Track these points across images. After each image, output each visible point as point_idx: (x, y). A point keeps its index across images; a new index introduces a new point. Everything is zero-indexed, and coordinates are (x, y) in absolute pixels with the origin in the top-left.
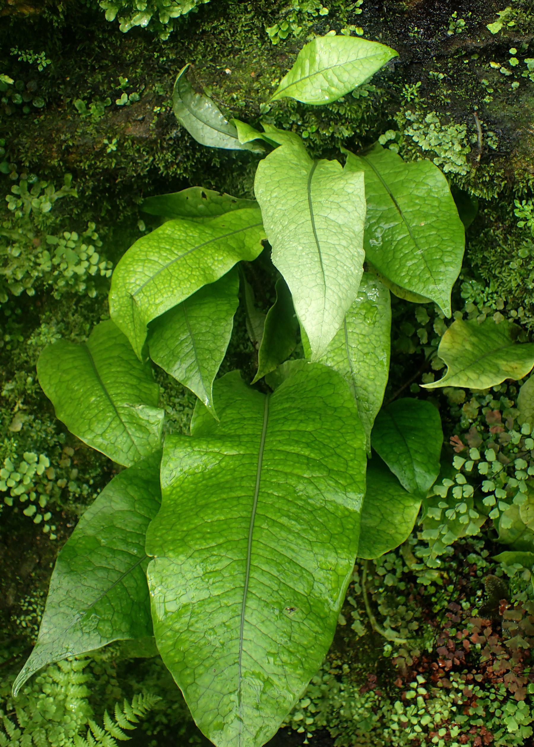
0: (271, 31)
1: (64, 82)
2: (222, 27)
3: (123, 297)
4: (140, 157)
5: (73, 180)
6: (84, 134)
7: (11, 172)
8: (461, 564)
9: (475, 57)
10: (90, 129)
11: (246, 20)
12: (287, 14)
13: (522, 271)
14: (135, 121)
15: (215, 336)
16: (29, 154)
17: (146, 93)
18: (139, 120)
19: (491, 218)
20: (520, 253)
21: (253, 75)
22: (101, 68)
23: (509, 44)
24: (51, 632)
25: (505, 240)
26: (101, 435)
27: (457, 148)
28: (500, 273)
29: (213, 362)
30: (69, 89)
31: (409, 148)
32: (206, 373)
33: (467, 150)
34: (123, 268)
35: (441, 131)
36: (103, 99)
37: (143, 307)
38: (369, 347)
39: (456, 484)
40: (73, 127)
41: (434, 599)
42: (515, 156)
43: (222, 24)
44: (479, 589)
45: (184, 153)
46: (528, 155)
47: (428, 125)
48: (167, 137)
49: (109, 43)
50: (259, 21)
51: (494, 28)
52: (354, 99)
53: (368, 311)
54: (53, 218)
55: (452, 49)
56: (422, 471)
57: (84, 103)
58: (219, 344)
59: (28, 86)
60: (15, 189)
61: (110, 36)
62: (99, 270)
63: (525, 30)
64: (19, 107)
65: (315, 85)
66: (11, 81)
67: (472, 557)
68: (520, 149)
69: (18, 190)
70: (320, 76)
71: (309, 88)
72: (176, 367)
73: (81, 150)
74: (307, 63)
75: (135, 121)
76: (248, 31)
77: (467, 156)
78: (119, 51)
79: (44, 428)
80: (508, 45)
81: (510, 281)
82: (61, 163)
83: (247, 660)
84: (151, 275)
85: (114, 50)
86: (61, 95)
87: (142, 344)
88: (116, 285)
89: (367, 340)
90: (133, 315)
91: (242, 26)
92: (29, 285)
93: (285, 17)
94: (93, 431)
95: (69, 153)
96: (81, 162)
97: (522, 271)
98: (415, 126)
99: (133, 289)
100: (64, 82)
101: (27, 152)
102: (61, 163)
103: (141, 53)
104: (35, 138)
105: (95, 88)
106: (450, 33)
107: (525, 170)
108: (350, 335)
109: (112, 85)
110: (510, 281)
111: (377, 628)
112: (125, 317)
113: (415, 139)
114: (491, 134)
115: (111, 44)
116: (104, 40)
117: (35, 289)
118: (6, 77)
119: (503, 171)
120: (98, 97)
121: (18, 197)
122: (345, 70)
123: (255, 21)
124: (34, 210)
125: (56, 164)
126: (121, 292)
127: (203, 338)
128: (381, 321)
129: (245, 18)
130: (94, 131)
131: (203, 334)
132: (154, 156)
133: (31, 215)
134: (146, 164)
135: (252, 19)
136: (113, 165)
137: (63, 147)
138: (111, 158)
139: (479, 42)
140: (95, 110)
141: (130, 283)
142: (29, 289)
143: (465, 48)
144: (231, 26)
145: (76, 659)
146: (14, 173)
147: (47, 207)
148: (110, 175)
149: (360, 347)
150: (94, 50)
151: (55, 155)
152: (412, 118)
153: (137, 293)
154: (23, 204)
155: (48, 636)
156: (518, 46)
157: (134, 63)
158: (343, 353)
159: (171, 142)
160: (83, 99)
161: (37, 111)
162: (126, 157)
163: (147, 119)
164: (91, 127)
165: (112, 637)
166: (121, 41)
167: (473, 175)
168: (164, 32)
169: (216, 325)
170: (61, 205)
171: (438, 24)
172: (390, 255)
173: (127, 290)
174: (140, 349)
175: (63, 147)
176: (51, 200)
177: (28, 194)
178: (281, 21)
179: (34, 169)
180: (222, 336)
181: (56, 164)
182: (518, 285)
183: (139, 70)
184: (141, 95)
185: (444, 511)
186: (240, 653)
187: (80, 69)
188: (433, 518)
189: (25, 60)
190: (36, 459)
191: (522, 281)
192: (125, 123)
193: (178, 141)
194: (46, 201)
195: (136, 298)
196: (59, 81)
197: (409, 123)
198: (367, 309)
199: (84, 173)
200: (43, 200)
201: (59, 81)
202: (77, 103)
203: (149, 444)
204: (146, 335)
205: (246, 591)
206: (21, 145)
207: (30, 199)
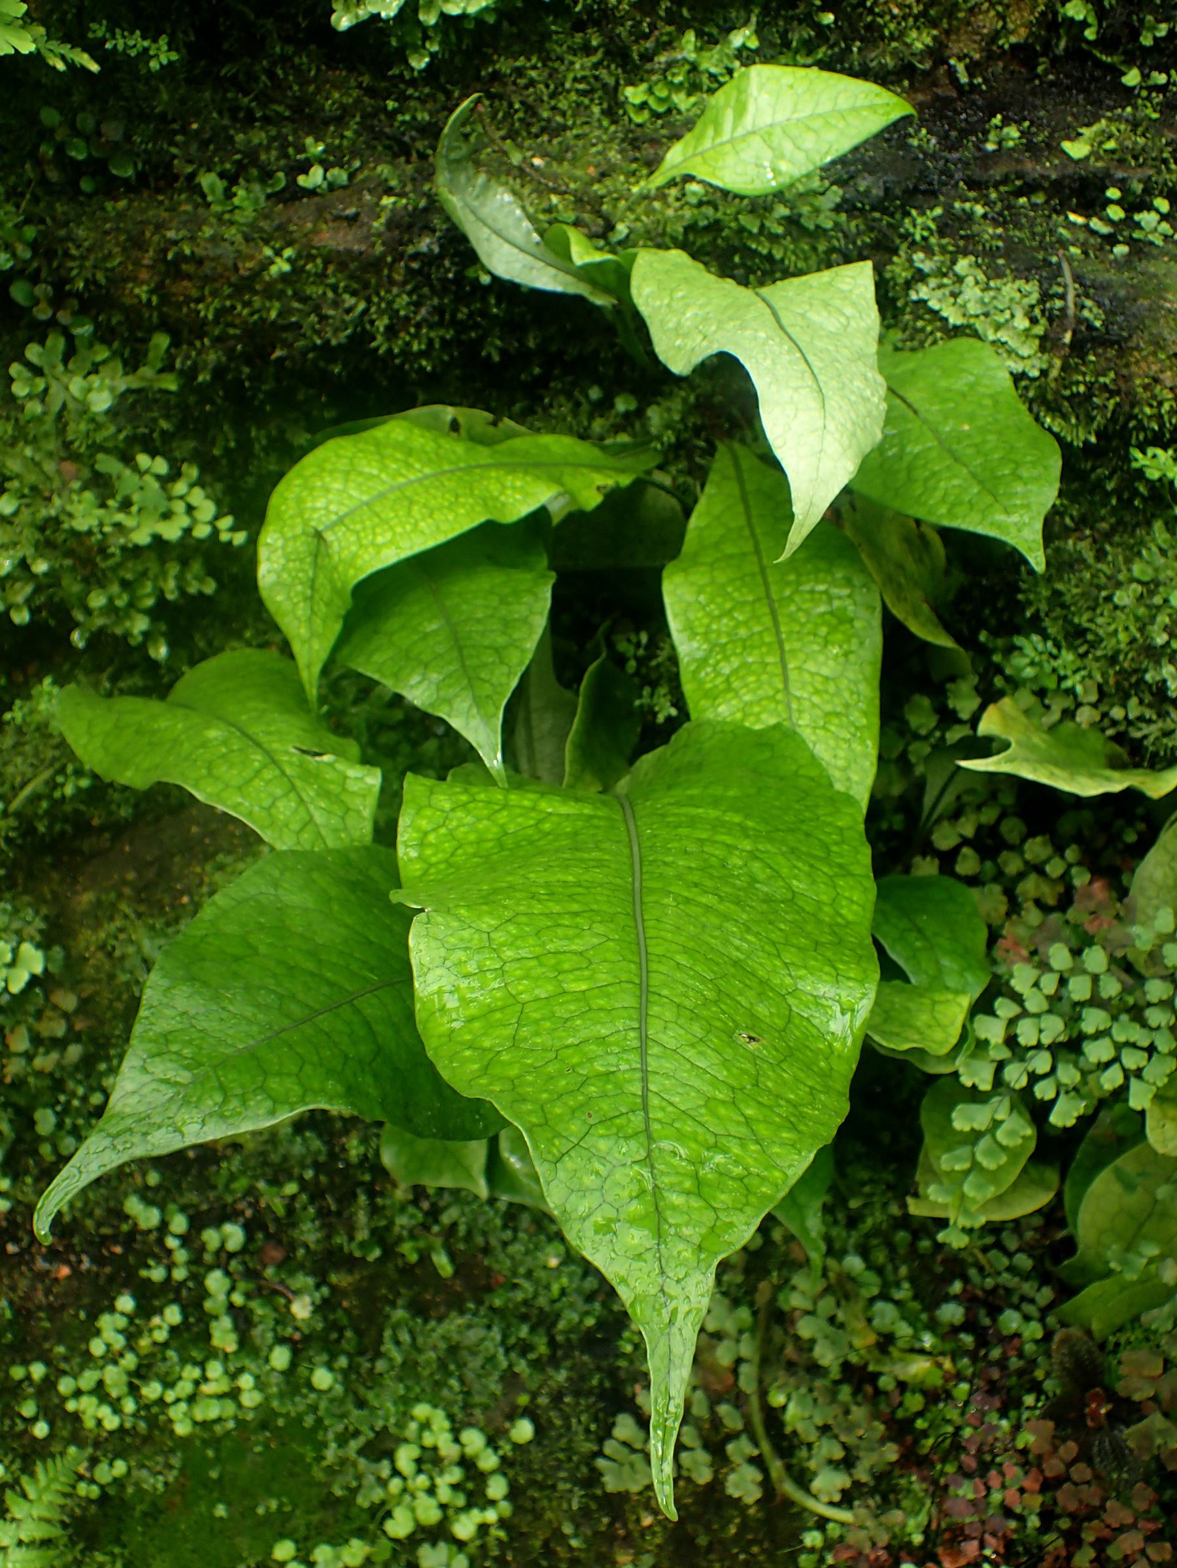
0: (634, 94)
1: (184, 130)
2: (533, 74)
3: (295, 538)
4: (336, 304)
5: (171, 345)
6: (215, 239)
7: (37, 302)
8: (983, 1340)
9: (1039, 199)
10: (231, 232)
11: (583, 68)
12: (670, 65)
13: (1142, 611)
14: (337, 218)
15: (507, 624)
16: (88, 264)
17: (360, 177)
18: (347, 218)
19: (1068, 521)
20: (1137, 569)
21: (592, 171)
22: (266, 120)
23: (1101, 181)
24: (146, 1090)
25: (1101, 555)
26: (240, 788)
27: (1022, 323)
28: (1091, 620)
29: (505, 669)
30: (193, 148)
31: (920, 324)
32: (487, 690)
33: (1039, 330)
34: (298, 482)
35: (987, 288)
36: (266, 176)
37: (345, 554)
38: (837, 701)
39: (1025, 1014)
40: (195, 223)
41: (920, 1424)
42: (1137, 348)
43: (534, 68)
44: (1029, 1391)
45: (436, 301)
46: (1162, 349)
47: (960, 279)
48: (411, 250)
49: (293, 67)
50: (611, 74)
51: (1076, 149)
52: (804, 231)
53: (833, 629)
54: (112, 429)
55: (997, 173)
56: (955, 966)
57: (220, 185)
58: (516, 635)
59: (104, 128)
60: (33, 352)
61: (298, 53)
62: (216, 532)
63: (1136, 158)
64: (76, 170)
65: (743, 156)
66: (94, 67)
67: (1011, 1321)
68: (1146, 335)
69: (40, 355)
70: (756, 141)
71: (730, 160)
72: (415, 679)
73: (207, 268)
74: (729, 115)
75: (337, 218)
76: (583, 93)
77: (1043, 339)
78: (312, 88)
79: (16, 925)
80: (1102, 180)
81: (1116, 632)
82: (155, 299)
83: (663, 1109)
84: (365, 498)
85: (301, 85)
86: (174, 157)
87: (324, 655)
88: (279, 516)
89: (831, 688)
90: (313, 581)
91: (575, 80)
92: (20, 599)
93: (665, 71)
94: (217, 779)
95: (179, 275)
96: (199, 300)
97: (1142, 611)
98: (933, 282)
99: (318, 520)
100: (184, 130)
101: (83, 258)
102: (155, 299)
103: (358, 101)
104: (107, 233)
105: (252, 155)
106: (990, 147)
107: (1156, 380)
108: (793, 675)
109: (291, 151)
110: (1116, 632)
111: (789, 1488)
112: (292, 586)
113: (934, 304)
114: (1089, 303)
115: (298, 70)
116: (285, 59)
117: (34, 612)
118: (86, 56)
119: (1112, 375)
120: (254, 172)
121: (37, 371)
122: (809, 128)
123: (603, 73)
124: (71, 406)
125: (144, 297)
126: (293, 527)
127: (480, 628)
128: (862, 652)
129: (581, 65)
130: (239, 238)
131: (478, 621)
132: (369, 301)
133: (60, 416)
134: (348, 318)
135: (596, 66)
136: (273, 314)
137: (170, 256)
138: (270, 298)
139: (1048, 168)
140: (247, 198)
141: (314, 509)
142: (18, 607)
143: (1020, 176)
144: (550, 76)
145: (20, 1543)
146: (43, 305)
147: (101, 402)
148: (261, 337)
149: (816, 699)
150: (257, 79)
151: (144, 275)
152: (927, 266)
153: (331, 527)
154: (46, 390)
155: (136, 1098)
156: (1122, 184)
157: (340, 120)
158: (780, 708)
159: (415, 265)
160: (222, 175)
161: (111, 187)
162: (305, 300)
163: (364, 218)
164: (233, 230)
165: (302, 1100)
166: (318, 69)
167: (1054, 373)
168: (418, 49)
169: (508, 604)
170: (133, 406)
171: (964, 133)
172: (902, 476)
173: (306, 523)
174: (317, 669)
175: (170, 256)
176: (112, 389)
177: (61, 368)
178: (654, 78)
179: (93, 303)
180: (525, 621)
181: (144, 297)
182: (1133, 641)
183: (348, 133)
184: (351, 176)
185: (1000, 1066)
186: (644, 1097)
187: (220, 113)
188: (974, 1086)
189: (120, 48)
190: (8, 957)
191: (1141, 630)
192: (315, 223)
193: (430, 264)
194: (100, 389)
195: (329, 536)
196: (176, 126)
197: (920, 277)
198: (829, 625)
199: (199, 329)
200: (96, 384)
201: (176, 126)
202: (209, 181)
203: (346, 829)
204: (338, 627)
205: (645, 992)
206: (73, 240)
207: (65, 379)
